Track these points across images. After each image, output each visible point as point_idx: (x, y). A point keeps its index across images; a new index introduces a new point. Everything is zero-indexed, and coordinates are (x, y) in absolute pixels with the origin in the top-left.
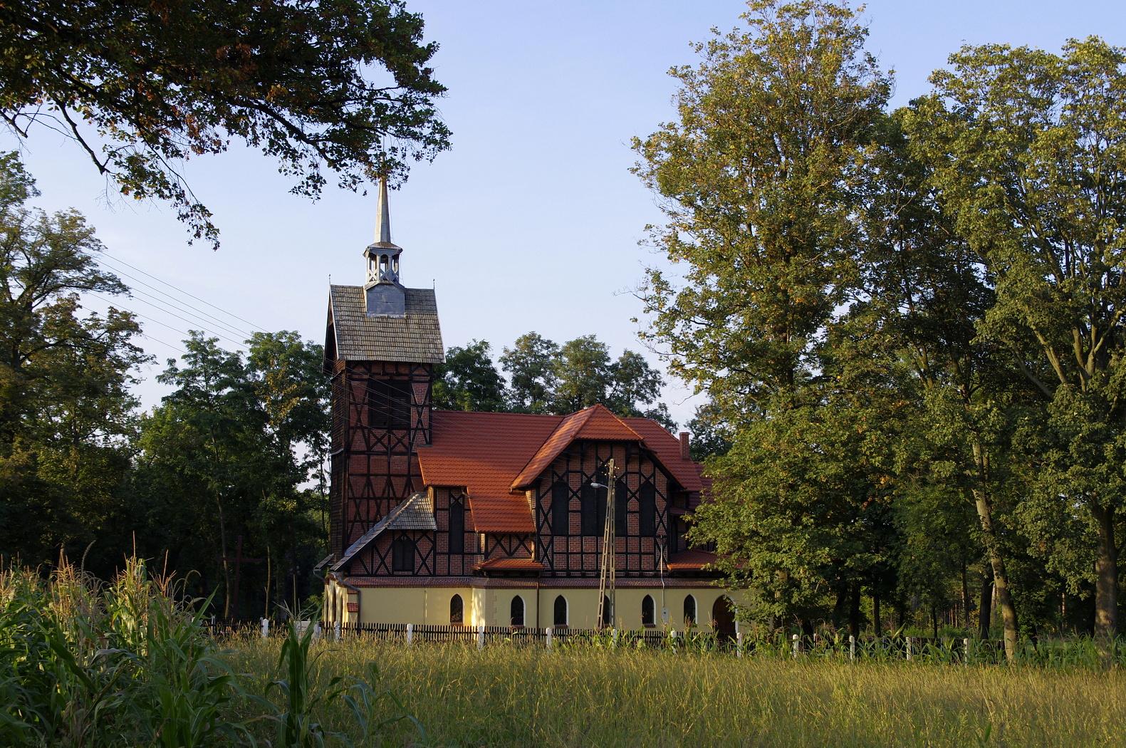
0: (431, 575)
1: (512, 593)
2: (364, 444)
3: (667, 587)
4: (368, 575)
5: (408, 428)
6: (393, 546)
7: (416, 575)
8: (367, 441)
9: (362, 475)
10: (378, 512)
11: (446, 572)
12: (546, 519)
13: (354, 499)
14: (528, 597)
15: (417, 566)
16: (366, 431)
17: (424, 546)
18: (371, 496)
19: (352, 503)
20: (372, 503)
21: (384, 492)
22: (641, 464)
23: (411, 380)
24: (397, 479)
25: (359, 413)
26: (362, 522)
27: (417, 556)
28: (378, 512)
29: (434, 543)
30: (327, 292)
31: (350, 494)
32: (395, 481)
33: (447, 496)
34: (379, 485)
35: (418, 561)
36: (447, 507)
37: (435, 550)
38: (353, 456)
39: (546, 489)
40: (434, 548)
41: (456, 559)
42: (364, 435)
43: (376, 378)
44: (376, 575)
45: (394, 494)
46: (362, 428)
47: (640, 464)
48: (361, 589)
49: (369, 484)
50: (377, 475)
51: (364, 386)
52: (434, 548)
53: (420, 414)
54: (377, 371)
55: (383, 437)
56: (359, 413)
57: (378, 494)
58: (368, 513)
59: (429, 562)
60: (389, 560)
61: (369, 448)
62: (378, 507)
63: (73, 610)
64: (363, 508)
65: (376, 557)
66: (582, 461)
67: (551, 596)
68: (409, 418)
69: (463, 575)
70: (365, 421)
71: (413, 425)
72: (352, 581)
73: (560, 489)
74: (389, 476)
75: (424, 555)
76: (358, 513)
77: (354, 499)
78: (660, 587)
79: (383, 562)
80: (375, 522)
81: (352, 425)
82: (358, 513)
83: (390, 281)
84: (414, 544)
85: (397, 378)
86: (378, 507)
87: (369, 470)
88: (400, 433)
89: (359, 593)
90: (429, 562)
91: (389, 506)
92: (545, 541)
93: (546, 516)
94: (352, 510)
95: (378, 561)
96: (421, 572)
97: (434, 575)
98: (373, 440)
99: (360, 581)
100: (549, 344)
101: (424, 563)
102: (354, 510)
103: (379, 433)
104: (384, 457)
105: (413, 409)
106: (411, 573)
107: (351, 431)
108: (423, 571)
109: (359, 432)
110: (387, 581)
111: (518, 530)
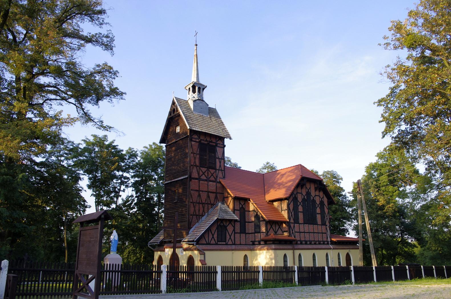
0: (233, 244)
2: (197, 175)
3: (333, 249)
5: (215, 169)
6: (217, 228)
7: (227, 244)
8: (199, 174)
9: (197, 191)
10: (204, 211)
11: (239, 243)
12: (292, 215)
13: (193, 203)
14: (289, 253)
15: (227, 239)
17: (230, 229)
19: (192, 205)
20: (201, 205)
21: (206, 200)
22: (319, 192)
23: (216, 145)
26: (197, 215)
27: (227, 234)
28: (204, 211)
29: (234, 227)
31: (191, 200)
33: (239, 203)
34: (204, 196)
35: (228, 237)
36: (239, 209)
37: (235, 232)
38: (192, 180)
40: (234, 230)
41: (243, 235)
42: (197, 170)
43: (202, 142)
44: (210, 244)
45: (210, 202)
46: (196, 166)
47: (319, 192)
49: (199, 195)
50: (202, 191)
52: (234, 230)
53: (220, 163)
55: (205, 172)
57: (204, 202)
59: (232, 237)
60: (215, 236)
61: (200, 177)
62: (204, 208)
64: (197, 208)
65: (210, 234)
66: (302, 188)
67: (297, 252)
68: (215, 163)
70: (198, 163)
73: (295, 199)
75: (230, 234)
77: (193, 203)
78: (331, 249)
79: (213, 237)
81: (192, 164)
84: (226, 227)
86: (204, 208)
88: (212, 171)
89: (204, 254)
90: (232, 237)
92: (292, 225)
94: (192, 209)
95: (211, 236)
97: (234, 244)
98: (201, 173)
99: (204, 247)
100: (96, 199)
102: (193, 209)
103: (204, 170)
104: (206, 182)
105: (217, 160)
106: (225, 243)
107: (192, 167)
108: (230, 242)
109: (195, 169)
111: (278, 219)
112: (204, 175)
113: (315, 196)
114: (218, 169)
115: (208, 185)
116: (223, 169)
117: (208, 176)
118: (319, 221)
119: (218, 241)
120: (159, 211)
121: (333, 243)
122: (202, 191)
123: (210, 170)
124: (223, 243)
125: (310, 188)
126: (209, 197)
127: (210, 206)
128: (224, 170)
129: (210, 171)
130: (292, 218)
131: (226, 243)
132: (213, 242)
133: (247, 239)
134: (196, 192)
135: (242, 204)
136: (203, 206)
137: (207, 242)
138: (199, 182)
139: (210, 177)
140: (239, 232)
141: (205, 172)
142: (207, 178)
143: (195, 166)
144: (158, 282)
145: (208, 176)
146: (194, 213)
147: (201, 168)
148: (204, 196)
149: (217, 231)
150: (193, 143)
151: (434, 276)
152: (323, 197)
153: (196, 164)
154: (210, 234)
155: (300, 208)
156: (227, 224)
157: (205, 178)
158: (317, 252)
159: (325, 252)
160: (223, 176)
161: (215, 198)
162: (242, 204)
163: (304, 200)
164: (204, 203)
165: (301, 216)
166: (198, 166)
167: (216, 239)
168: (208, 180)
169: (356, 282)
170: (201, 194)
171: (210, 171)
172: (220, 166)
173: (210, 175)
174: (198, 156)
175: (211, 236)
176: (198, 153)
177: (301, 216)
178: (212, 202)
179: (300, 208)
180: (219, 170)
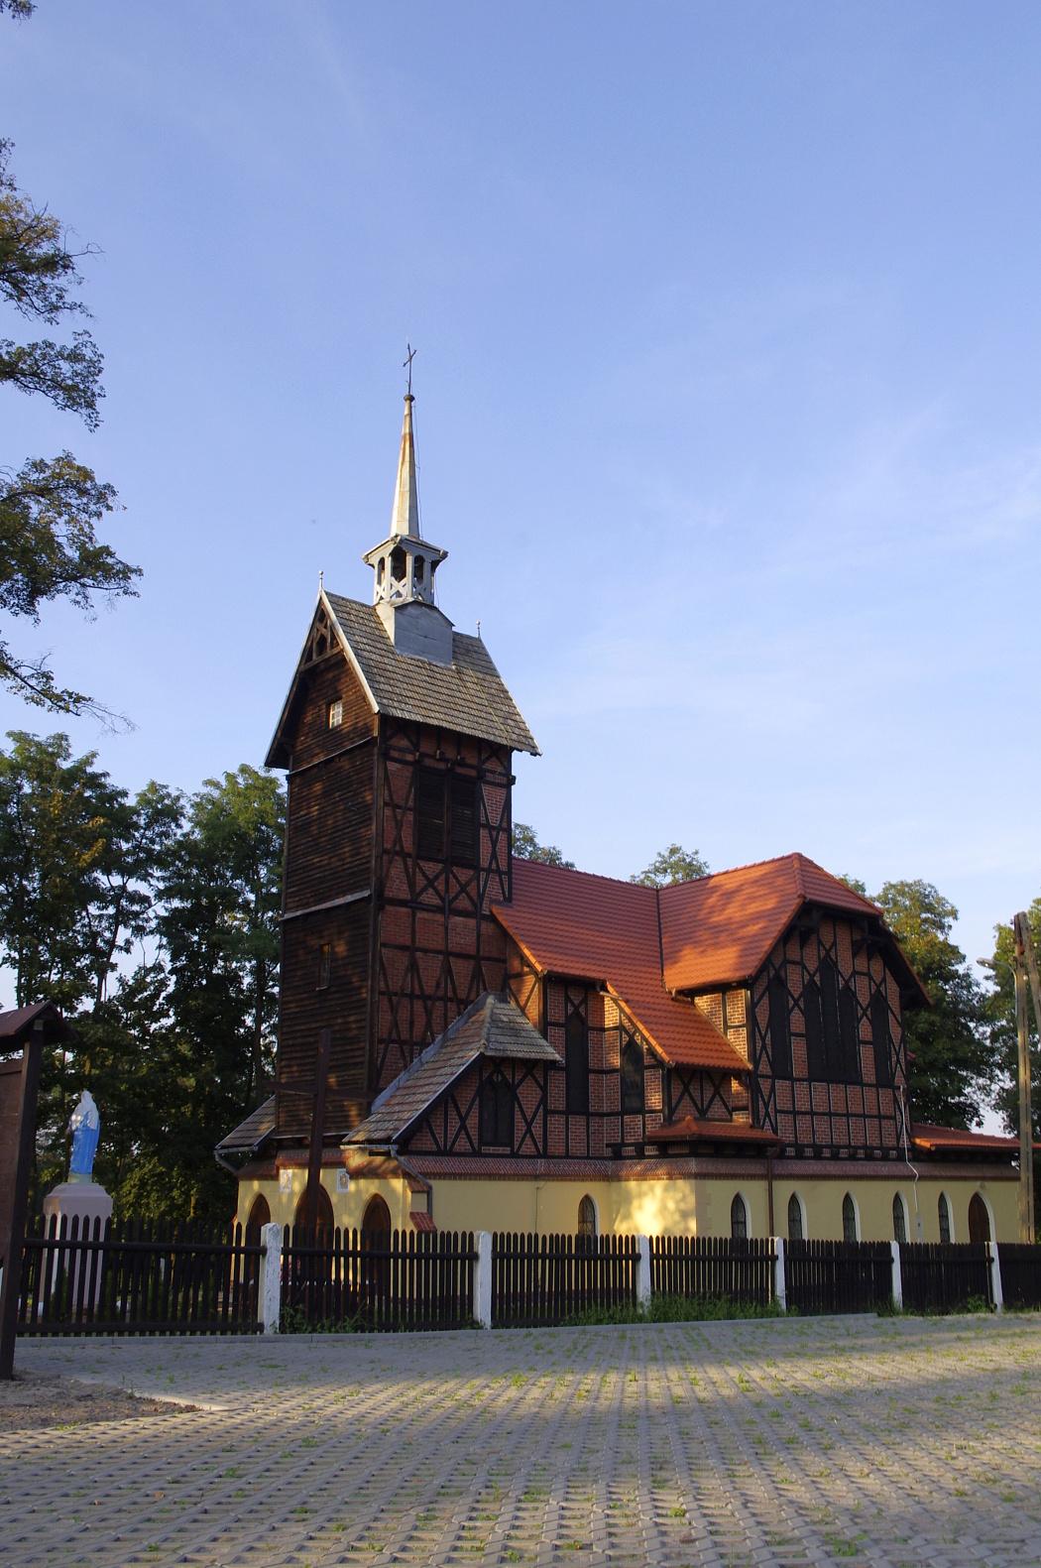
0: (539, 1156)
1: (973, 1187)
2: (405, 887)
3: (922, 1178)
4: (440, 1153)
5: (474, 865)
6: (480, 1093)
7: (514, 1155)
8: (412, 884)
9: (403, 948)
10: (429, 1025)
11: (562, 1151)
14: (753, 1192)
15: (518, 1134)
16: (410, 861)
17: (528, 1095)
18: (417, 992)
19: (385, 1004)
20: (418, 1006)
21: (438, 985)
24: (460, 962)
25: (399, 825)
26: (402, 1043)
27: (518, 1116)
28: (429, 1025)
29: (544, 1089)
30: (442, 547)
32: (457, 965)
34: (431, 970)
35: (520, 1126)
36: (562, 1020)
37: (545, 1107)
38: (388, 908)
39: (761, 991)
40: (544, 1100)
41: (578, 1123)
42: (407, 870)
43: (428, 762)
45: (421, 988)
46: (405, 855)
47: (869, 960)
48: (433, 1183)
49: (413, 967)
50: (425, 951)
51: (408, 772)
52: (544, 1100)
54: (430, 751)
55: (437, 877)
56: (399, 825)
57: (429, 991)
58: (412, 1024)
59: (537, 1130)
60: (472, 1122)
62: (428, 1012)
63: (574, 1361)
64: (403, 1015)
69: (588, 1158)
70: (408, 844)
71: (484, 862)
72: (417, 1164)
73: (778, 985)
76: (395, 1024)
78: (911, 1178)
79: (463, 1127)
81: (388, 846)
82: (395, 1024)
83: (420, 609)
84: (511, 1088)
85: (460, 770)
86: (428, 1012)
87: (413, 941)
88: (464, 875)
89: (429, 1192)
90: (537, 1130)
91: (445, 1015)
93: (763, 1039)
94: (384, 1018)
95: (455, 1124)
96: (524, 1150)
98: (421, 881)
101: (529, 1130)
102: (388, 1017)
103: (431, 868)
104: (439, 917)
105: (483, 833)
106: (508, 1150)
107: (385, 857)
109: (399, 863)
110: (475, 1164)
112: (431, 890)
113: (855, 973)
116: (504, 868)
117: (447, 891)
118: (868, 1072)
119: (482, 1143)
122: (425, 951)
125: (834, 944)
126: (448, 972)
128: (509, 873)
129: (455, 877)
131: (512, 1150)
132: (462, 1145)
135: (576, 1002)
136: (425, 1008)
137: (442, 1144)
138: (414, 916)
140: (562, 1106)
141: (437, 877)
142: (442, 899)
143: (397, 853)
145: (447, 891)
146: (390, 1033)
147: (422, 863)
148: (431, 970)
149: (477, 1102)
152: (884, 980)
154: (453, 1114)
155: (797, 1021)
156: (518, 1078)
157: (437, 901)
158: (860, 1191)
159: (892, 1187)
160: (504, 893)
162: (576, 1002)
163: (810, 989)
165: (799, 1050)
166: (409, 855)
168: (447, 909)
169: (1010, 1303)
171: (455, 877)
172: (494, 856)
173: (455, 888)
174: (410, 817)
176: (411, 804)
177: (799, 1050)
179: (797, 1021)
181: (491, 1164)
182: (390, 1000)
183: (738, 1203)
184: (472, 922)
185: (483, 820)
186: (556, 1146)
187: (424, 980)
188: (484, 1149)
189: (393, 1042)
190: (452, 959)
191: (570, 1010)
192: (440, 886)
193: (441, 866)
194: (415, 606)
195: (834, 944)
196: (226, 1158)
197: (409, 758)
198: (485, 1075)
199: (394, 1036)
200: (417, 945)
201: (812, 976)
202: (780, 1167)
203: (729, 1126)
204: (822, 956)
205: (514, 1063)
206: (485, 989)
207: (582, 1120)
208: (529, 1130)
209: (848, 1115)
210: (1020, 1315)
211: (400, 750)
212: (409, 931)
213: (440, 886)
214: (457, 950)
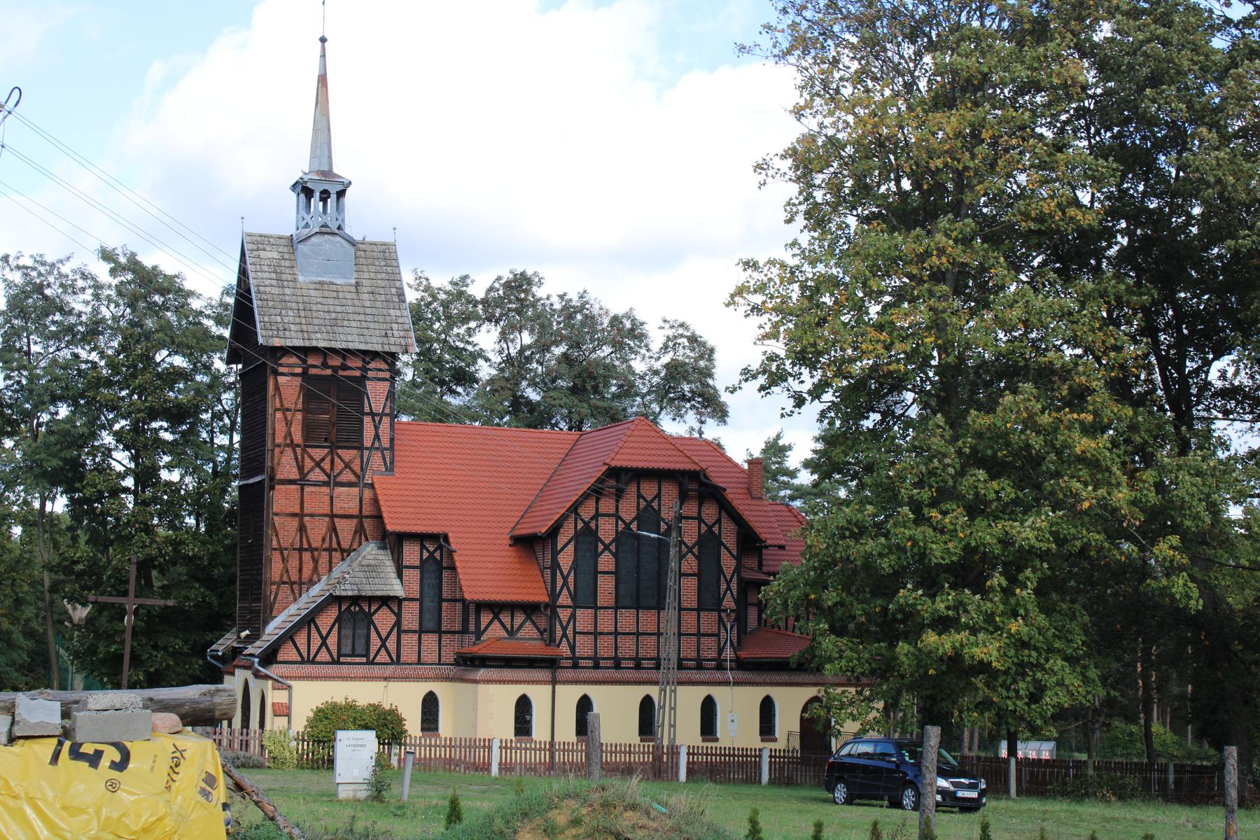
0: (392, 663)
2: (295, 470)
3: (737, 683)
4: (303, 662)
5: (360, 448)
6: (338, 620)
8: (301, 469)
9: (294, 515)
10: (315, 569)
11: (415, 659)
14: (539, 695)
15: (373, 649)
16: (299, 450)
17: (384, 619)
20: (307, 556)
21: (324, 540)
24: (343, 521)
25: (289, 424)
27: (373, 635)
28: (315, 569)
29: (399, 615)
34: (317, 530)
35: (375, 642)
36: (417, 563)
40: (398, 623)
42: (296, 458)
43: (312, 371)
44: (313, 662)
45: (339, 543)
49: (302, 529)
50: (312, 515)
52: (398, 623)
55: (323, 460)
56: (289, 424)
59: (392, 644)
60: (332, 641)
62: (315, 561)
64: (293, 563)
70: (298, 437)
71: (367, 442)
74: (332, 516)
80: (311, 583)
86: (315, 561)
88: (348, 454)
90: (392, 644)
91: (330, 561)
95: (316, 641)
97: (398, 662)
98: (308, 464)
103: (318, 453)
104: (325, 490)
105: (367, 419)
106: (364, 660)
108: (383, 657)
112: (317, 470)
113: (680, 518)
114: (369, 445)
115: (332, 498)
117: (332, 469)
119: (339, 655)
120: (237, 446)
121: (741, 665)
122: (312, 515)
123: (340, 451)
124: (358, 660)
125: (658, 496)
126: (334, 529)
127: (336, 555)
128: (392, 448)
129: (339, 457)
130: (565, 591)
133: (443, 649)
134: (290, 519)
135: (431, 549)
136: (313, 557)
137: (305, 655)
138: (302, 490)
139: (340, 474)
140: (416, 626)
141: (323, 460)
142: (329, 476)
143: (287, 445)
144: (1019, 771)
145: (332, 469)
146: (282, 576)
147: (309, 450)
148: (317, 530)
150: (281, 379)
151: (1007, 791)
152: (719, 521)
153: (292, 441)
154: (314, 634)
155: (606, 561)
156: (373, 608)
157: (323, 478)
158: (777, 693)
160: (385, 464)
161: (355, 533)
162: (431, 549)
163: (624, 538)
164: (316, 549)
165: (606, 586)
166: (298, 446)
167: (334, 649)
168: (332, 482)
169: (1018, 793)
170: (308, 524)
171: (339, 457)
172: (377, 437)
173: (339, 465)
174: (299, 416)
175: (316, 641)
176: (300, 406)
177: (606, 586)
178: (345, 545)
179: (606, 561)
180: (382, 415)
181: (345, 669)
182: (282, 554)
183: (523, 706)
184: (355, 490)
185: (367, 409)
186: (409, 653)
187: (311, 537)
188: (342, 659)
189: (284, 583)
190: (336, 520)
191: (426, 555)
192: (326, 465)
193: (327, 450)
194: (319, 236)
195: (658, 496)
196: (212, 657)
197: (299, 370)
198: (343, 608)
199: (285, 579)
200: (305, 511)
201: (627, 526)
202: (561, 674)
203: (218, 691)
204: (641, 506)
205: (371, 599)
206: (367, 540)
207: (435, 637)
208: (383, 645)
209: (638, 634)
210: (1080, 809)
211: (289, 366)
212: (298, 502)
213: (326, 465)
214: (342, 512)
